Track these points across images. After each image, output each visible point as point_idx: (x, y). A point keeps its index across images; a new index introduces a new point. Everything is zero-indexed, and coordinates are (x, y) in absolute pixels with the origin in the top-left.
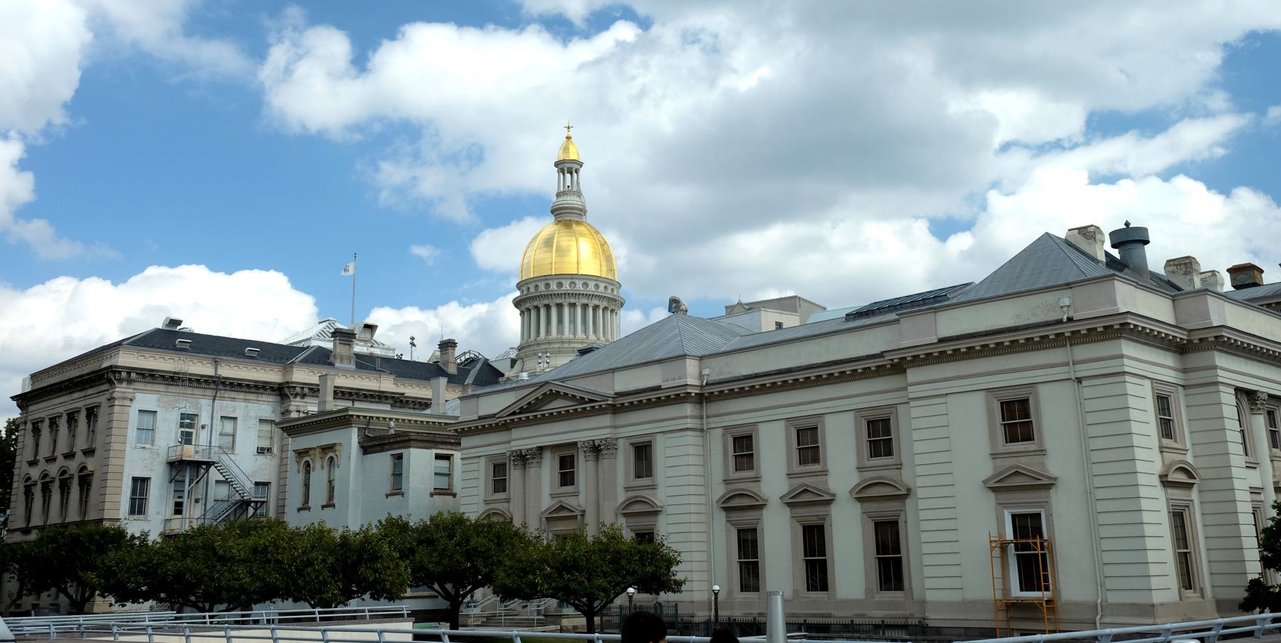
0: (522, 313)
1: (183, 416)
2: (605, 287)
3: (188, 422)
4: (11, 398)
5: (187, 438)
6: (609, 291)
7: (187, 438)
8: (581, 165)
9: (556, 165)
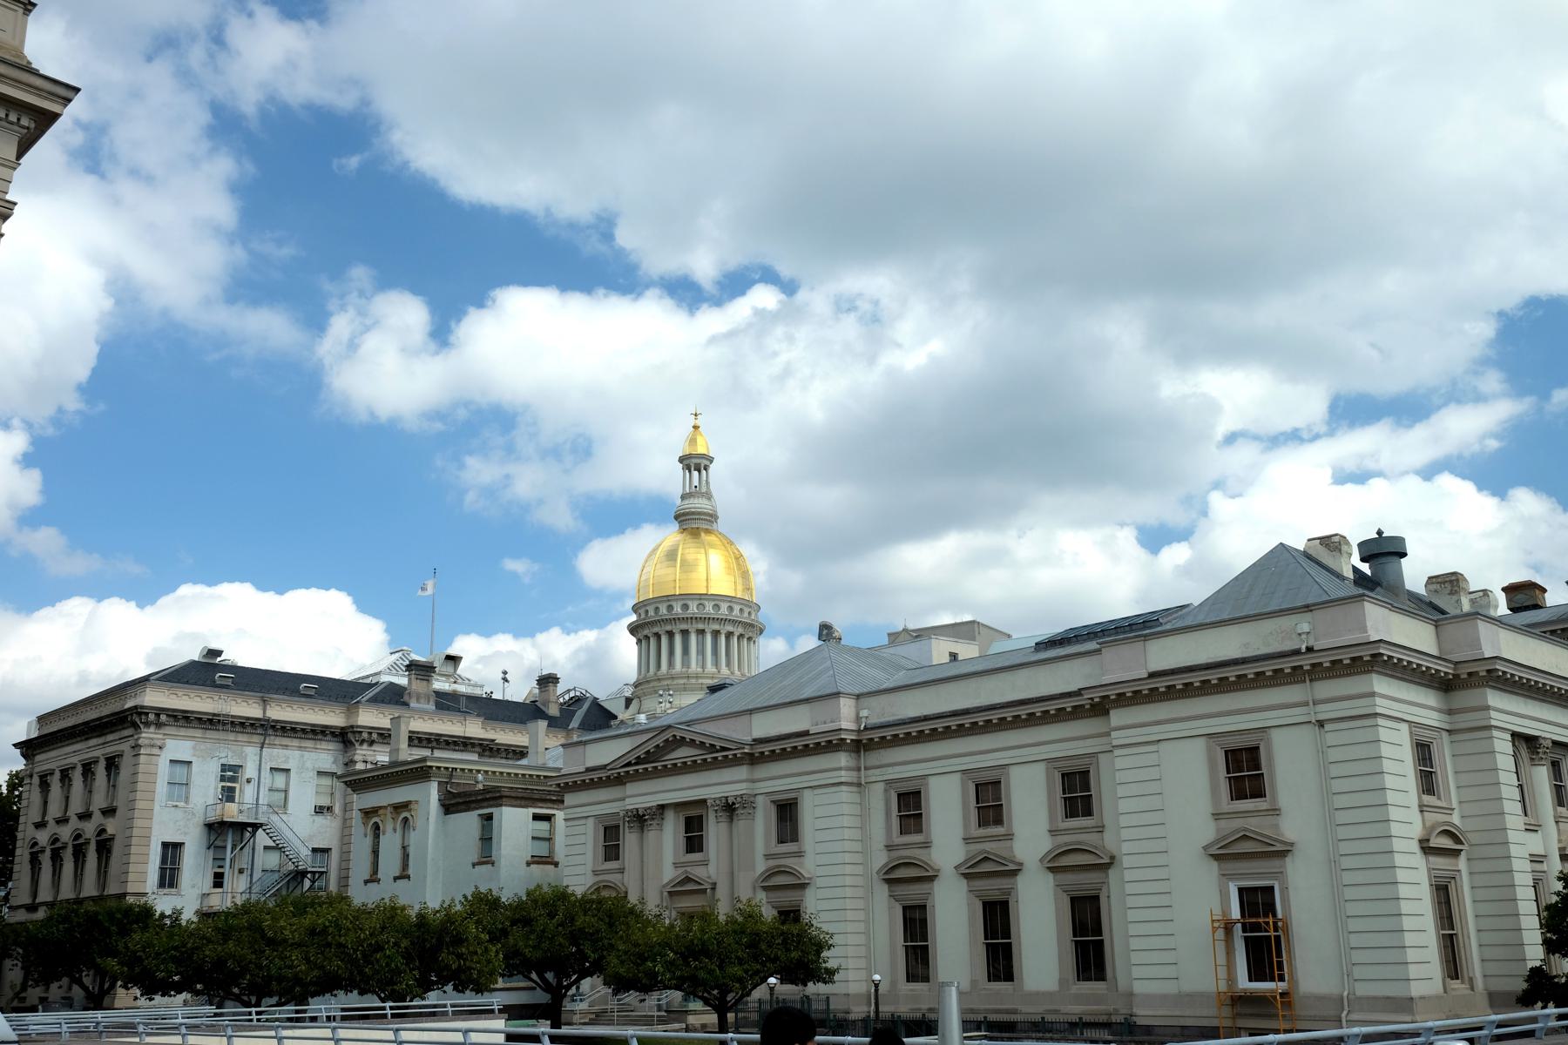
0: (639, 642)
1: (224, 768)
2: (741, 610)
3: (230, 774)
4: (14, 745)
5: (229, 795)
6: (746, 615)
7: (229, 795)
8: (711, 460)
9: (681, 460)
